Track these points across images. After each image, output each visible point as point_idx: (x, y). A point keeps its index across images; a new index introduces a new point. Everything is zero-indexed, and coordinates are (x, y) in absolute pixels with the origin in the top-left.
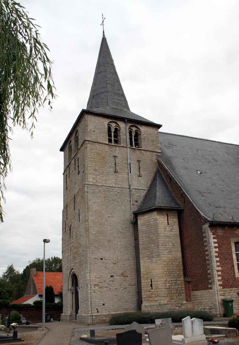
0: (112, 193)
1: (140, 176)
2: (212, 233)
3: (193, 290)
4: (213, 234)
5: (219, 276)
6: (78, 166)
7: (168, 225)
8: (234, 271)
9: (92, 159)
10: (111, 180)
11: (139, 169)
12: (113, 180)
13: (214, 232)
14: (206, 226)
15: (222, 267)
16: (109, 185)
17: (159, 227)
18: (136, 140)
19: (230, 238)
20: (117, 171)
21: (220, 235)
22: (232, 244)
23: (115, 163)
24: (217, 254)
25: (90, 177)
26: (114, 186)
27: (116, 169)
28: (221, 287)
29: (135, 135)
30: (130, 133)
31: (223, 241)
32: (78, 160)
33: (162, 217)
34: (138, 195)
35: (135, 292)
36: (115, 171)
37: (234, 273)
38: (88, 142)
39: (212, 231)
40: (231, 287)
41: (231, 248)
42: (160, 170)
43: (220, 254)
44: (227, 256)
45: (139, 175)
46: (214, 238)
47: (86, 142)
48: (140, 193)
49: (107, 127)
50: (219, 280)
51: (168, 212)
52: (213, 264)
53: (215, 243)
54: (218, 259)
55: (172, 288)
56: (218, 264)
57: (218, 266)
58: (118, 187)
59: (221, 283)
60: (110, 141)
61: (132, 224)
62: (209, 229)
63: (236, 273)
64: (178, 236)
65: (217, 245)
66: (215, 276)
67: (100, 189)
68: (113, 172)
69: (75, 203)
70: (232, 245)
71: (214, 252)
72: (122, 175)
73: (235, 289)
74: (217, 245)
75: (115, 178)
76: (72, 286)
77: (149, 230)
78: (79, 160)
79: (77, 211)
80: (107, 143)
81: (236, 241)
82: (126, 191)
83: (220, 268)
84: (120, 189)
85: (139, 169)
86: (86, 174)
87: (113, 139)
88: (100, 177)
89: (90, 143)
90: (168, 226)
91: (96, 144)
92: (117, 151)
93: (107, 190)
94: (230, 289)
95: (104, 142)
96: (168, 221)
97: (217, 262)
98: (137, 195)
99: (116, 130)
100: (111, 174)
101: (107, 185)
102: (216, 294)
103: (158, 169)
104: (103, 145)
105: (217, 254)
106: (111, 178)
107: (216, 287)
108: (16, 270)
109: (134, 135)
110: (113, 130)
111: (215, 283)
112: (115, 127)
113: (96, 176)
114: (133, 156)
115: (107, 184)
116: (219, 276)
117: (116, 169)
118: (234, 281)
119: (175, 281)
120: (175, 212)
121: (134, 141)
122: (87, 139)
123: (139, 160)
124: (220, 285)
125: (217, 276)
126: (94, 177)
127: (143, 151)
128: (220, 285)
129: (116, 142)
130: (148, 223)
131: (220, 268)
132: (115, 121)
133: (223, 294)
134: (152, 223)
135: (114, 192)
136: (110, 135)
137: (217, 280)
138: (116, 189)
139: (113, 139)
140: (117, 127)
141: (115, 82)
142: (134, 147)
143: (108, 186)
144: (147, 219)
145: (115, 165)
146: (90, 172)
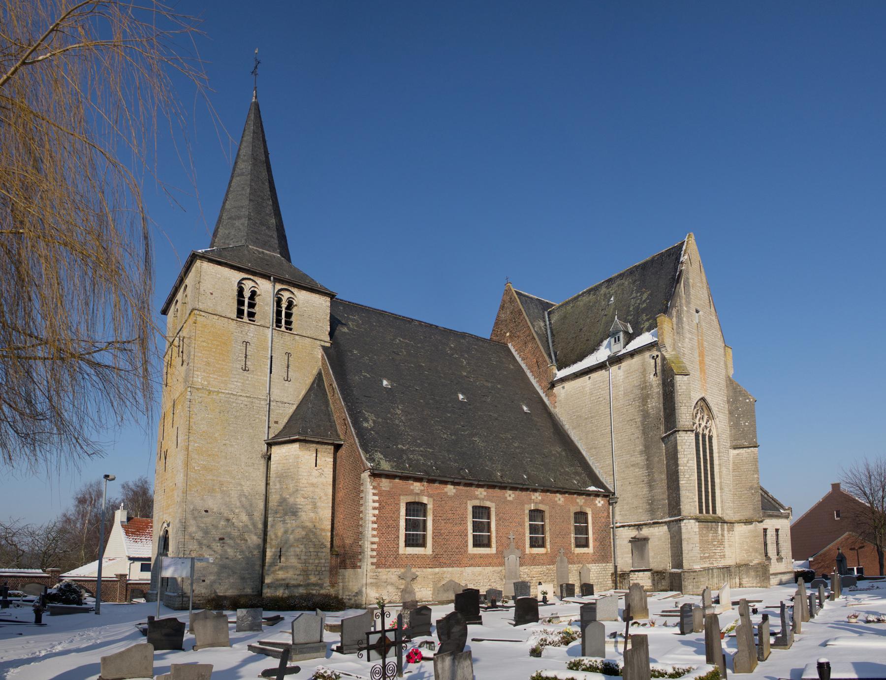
0: (234, 405)
1: (287, 380)
2: (372, 487)
3: (340, 569)
4: (374, 488)
5: (373, 550)
6: (182, 352)
7: (316, 466)
8: (398, 544)
9: (204, 344)
10: (235, 383)
11: (288, 367)
12: (239, 384)
13: (376, 485)
14: (366, 475)
15: (380, 538)
16: (230, 392)
17: (300, 469)
18: (289, 315)
19: (400, 495)
20: (247, 369)
21: (384, 491)
22: (401, 504)
23: (246, 355)
24: (375, 519)
25: (198, 375)
26: (238, 394)
27: (245, 364)
28: (374, 567)
29: (288, 306)
30: (279, 302)
31: (389, 499)
32: (183, 339)
33: (308, 453)
34: (281, 412)
35: (359, 593)
36: (244, 368)
37: (398, 548)
38: (198, 313)
39: (373, 484)
40: (390, 566)
41: (398, 510)
42: (323, 372)
43: (379, 519)
44: (391, 522)
45: (286, 379)
46: (374, 494)
47: (196, 312)
48: (283, 409)
49: (236, 288)
50: (372, 557)
51: (319, 447)
52: (367, 532)
53: (374, 501)
54: (375, 526)
55: (309, 563)
56: (375, 533)
57: (374, 536)
58: (247, 397)
59: (375, 560)
60: (240, 313)
61: (263, 459)
62: (369, 480)
63: (400, 548)
64: (330, 484)
65: (377, 505)
66: (366, 550)
67: (214, 397)
68: (241, 370)
69: (173, 414)
70: (402, 507)
71: (372, 515)
72: (255, 376)
73: (395, 570)
74: (377, 505)
75: (242, 381)
76: (164, 549)
77: (285, 472)
78: (185, 340)
79: (175, 428)
80: (234, 316)
81: (408, 501)
82: (260, 404)
83: (376, 540)
84: (249, 399)
85: (288, 367)
86: (191, 370)
87: (246, 308)
88: (215, 377)
89: (203, 314)
90: (316, 468)
91: (215, 316)
92: (250, 331)
93: (226, 399)
94: (387, 570)
95: (229, 315)
96: (316, 460)
97: (373, 529)
98: (278, 411)
99: (253, 294)
100: (235, 373)
101: (227, 392)
102: (365, 576)
103: (320, 369)
104: (226, 319)
105: (375, 519)
106: (236, 380)
107: (365, 567)
108: (705, 674)
109: (286, 306)
110: (247, 294)
111: (366, 560)
112: (253, 289)
113: (210, 374)
114: (278, 344)
115: (226, 389)
116: (373, 550)
117: (245, 364)
118: (396, 558)
119: (315, 553)
120: (330, 447)
121: (286, 317)
122: (197, 307)
123: (289, 352)
124: (372, 564)
125: (369, 550)
126: (205, 375)
127: (297, 337)
128: (372, 564)
129: (251, 315)
130: (285, 461)
131: (376, 540)
132: (252, 277)
133: (374, 577)
134: (290, 461)
135: (237, 403)
136: (241, 303)
137: (369, 557)
138: (243, 399)
139: (246, 308)
140: (256, 289)
141: (265, 198)
142: (283, 329)
143: (229, 393)
144: (285, 455)
145: (246, 357)
146: (199, 365)
